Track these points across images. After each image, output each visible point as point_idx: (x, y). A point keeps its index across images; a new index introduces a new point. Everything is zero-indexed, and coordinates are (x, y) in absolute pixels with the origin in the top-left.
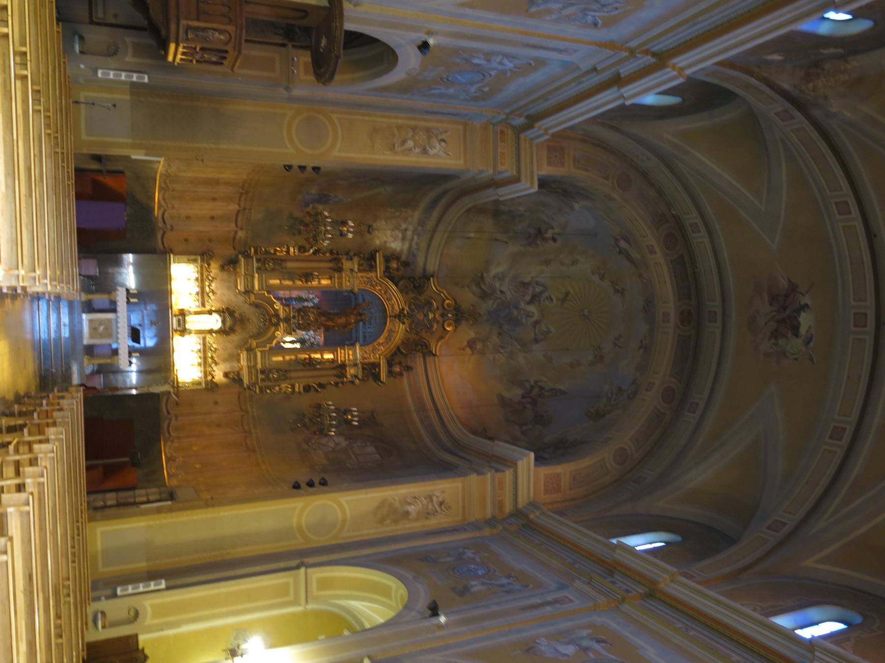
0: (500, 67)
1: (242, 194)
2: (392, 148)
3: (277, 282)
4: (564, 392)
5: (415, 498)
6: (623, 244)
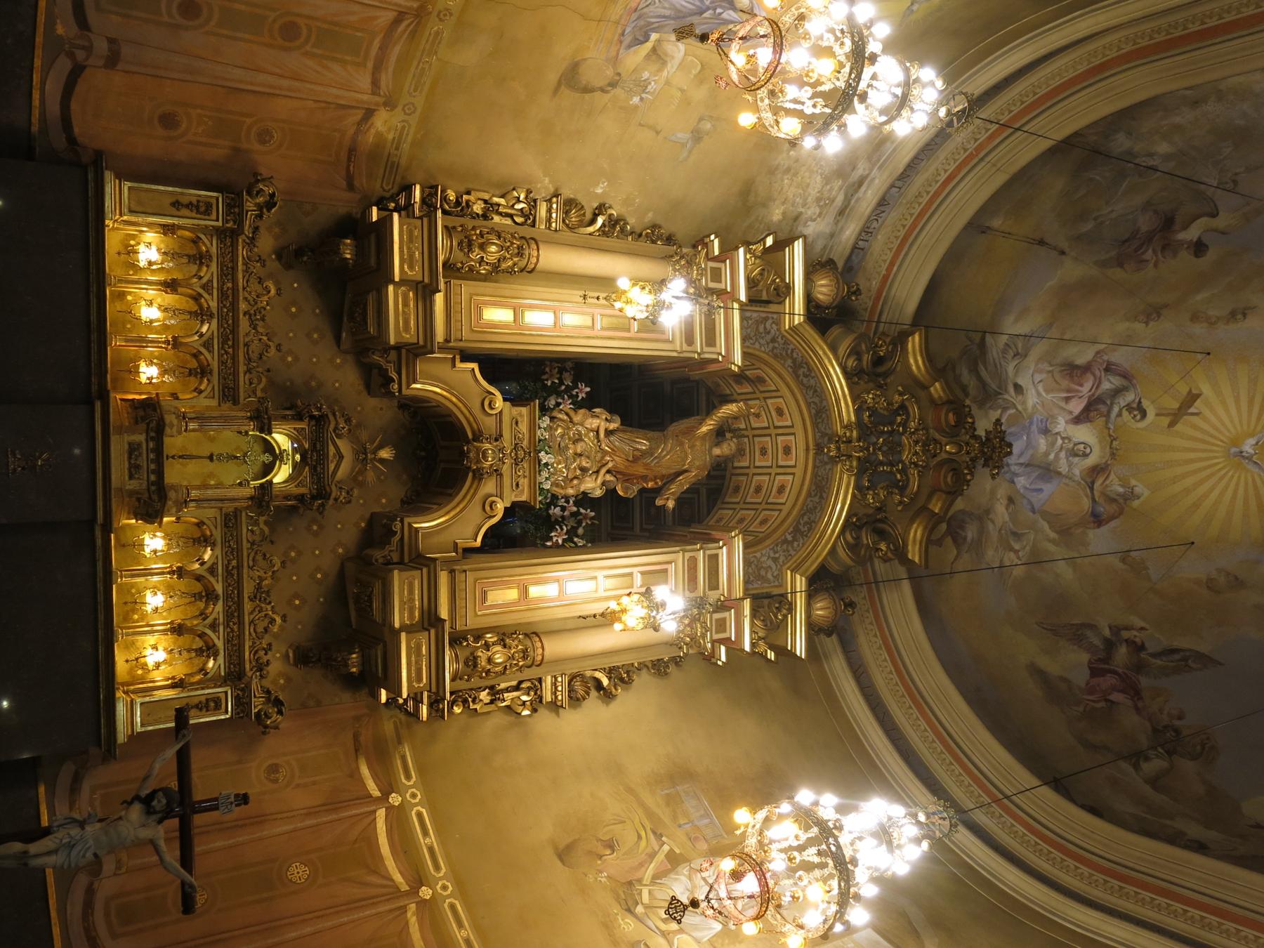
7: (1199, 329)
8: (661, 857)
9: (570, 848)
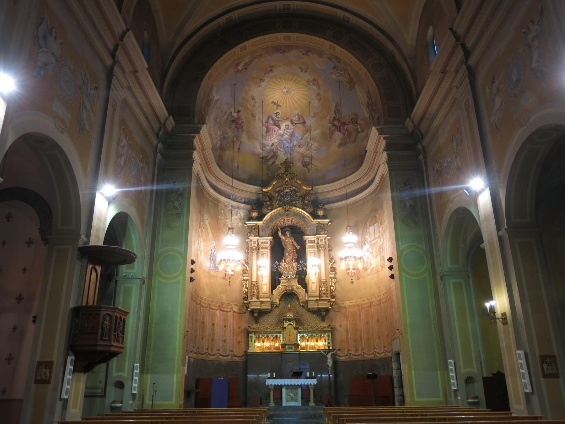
0: (126, 148)
1: (210, 308)
4: (337, 106)
6: (240, 67)
7: (257, 105)
9: (358, 277)
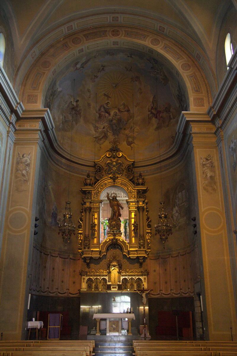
2: (26, 181)
3: (95, 239)
5: (203, 173)
6: (78, 66)
8: (171, 219)
